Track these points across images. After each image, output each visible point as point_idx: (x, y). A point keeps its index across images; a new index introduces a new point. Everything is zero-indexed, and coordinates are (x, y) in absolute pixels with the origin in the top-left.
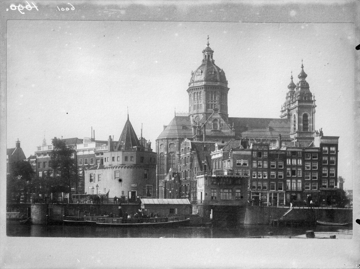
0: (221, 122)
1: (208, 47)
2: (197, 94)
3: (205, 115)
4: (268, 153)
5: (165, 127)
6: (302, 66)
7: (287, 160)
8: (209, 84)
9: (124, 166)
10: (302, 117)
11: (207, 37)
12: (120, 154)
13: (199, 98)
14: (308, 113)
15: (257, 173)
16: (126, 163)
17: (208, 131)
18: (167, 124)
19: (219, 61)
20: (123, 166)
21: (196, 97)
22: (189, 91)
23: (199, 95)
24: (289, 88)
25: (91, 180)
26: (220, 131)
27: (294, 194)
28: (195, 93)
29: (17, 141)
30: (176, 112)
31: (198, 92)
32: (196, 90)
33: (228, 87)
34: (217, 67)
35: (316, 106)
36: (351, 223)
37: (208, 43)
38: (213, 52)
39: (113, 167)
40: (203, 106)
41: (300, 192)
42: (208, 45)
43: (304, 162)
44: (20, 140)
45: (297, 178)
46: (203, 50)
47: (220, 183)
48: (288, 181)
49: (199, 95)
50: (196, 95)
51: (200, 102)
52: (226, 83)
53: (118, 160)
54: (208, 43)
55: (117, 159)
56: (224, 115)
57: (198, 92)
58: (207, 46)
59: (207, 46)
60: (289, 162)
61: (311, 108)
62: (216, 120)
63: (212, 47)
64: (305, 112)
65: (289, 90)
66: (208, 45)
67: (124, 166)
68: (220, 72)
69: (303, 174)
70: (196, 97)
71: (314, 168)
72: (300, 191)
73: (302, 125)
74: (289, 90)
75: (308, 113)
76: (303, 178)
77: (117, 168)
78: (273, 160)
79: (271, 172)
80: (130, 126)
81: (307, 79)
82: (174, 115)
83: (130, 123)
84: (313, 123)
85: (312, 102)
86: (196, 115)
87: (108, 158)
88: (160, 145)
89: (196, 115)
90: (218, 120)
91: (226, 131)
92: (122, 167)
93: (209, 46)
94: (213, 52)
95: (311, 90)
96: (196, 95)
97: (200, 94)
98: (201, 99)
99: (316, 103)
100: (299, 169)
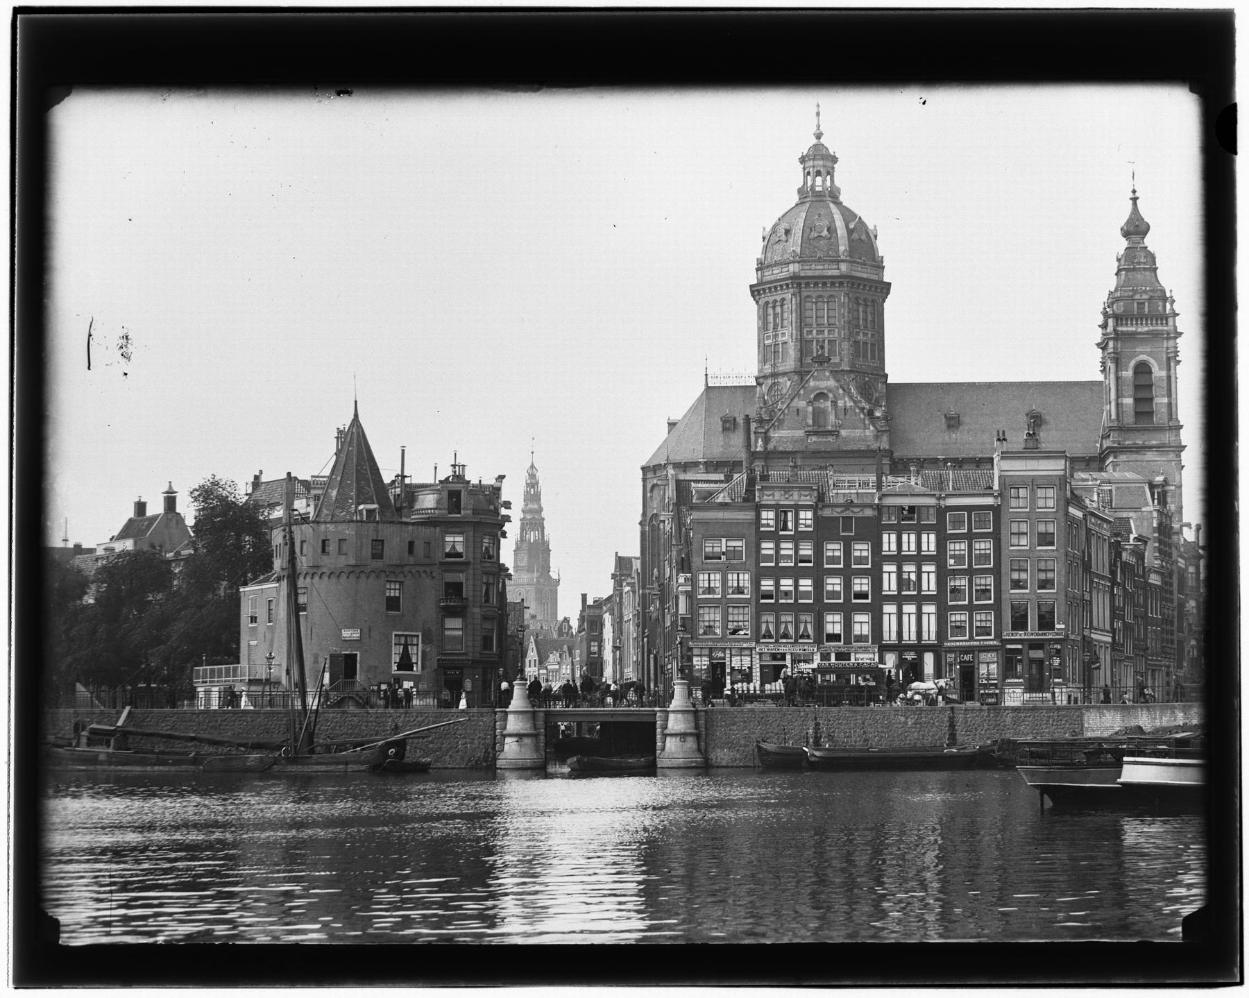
0: (840, 403)
2: (774, 307)
3: (796, 378)
4: (815, 514)
5: (672, 425)
6: (1131, 195)
7: (885, 537)
8: (810, 273)
9: (358, 570)
10: (1128, 374)
11: (815, 110)
14: (1152, 361)
17: (784, 436)
18: (677, 416)
19: (857, 190)
21: (771, 318)
23: (778, 310)
24: (1126, 234)
26: (835, 433)
27: (910, 656)
28: (767, 303)
29: (166, 489)
31: (783, 300)
33: (886, 279)
34: (848, 215)
38: (834, 159)
40: (792, 352)
41: (929, 648)
42: (819, 136)
45: (920, 600)
48: (890, 608)
49: (778, 310)
50: (770, 311)
51: (783, 334)
52: (879, 266)
53: (344, 549)
57: (783, 300)
58: (814, 141)
59: (814, 141)
60: (889, 542)
62: (821, 395)
63: (832, 144)
64: (1143, 357)
65: (1124, 243)
66: (819, 136)
67: (358, 570)
68: (852, 226)
69: (941, 583)
70: (771, 318)
73: (1128, 401)
74: (1124, 243)
75: (1152, 361)
76: (938, 599)
78: (835, 538)
79: (763, 583)
80: (358, 436)
83: (360, 427)
84: (1169, 395)
85: (1164, 318)
86: (769, 382)
88: (649, 487)
89: (769, 382)
90: (831, 395)
93: (822, 141)
94: (834, 159)
96: (770, 311)
97: (782, 306)
98: (785, 323)
100: (925, 568)
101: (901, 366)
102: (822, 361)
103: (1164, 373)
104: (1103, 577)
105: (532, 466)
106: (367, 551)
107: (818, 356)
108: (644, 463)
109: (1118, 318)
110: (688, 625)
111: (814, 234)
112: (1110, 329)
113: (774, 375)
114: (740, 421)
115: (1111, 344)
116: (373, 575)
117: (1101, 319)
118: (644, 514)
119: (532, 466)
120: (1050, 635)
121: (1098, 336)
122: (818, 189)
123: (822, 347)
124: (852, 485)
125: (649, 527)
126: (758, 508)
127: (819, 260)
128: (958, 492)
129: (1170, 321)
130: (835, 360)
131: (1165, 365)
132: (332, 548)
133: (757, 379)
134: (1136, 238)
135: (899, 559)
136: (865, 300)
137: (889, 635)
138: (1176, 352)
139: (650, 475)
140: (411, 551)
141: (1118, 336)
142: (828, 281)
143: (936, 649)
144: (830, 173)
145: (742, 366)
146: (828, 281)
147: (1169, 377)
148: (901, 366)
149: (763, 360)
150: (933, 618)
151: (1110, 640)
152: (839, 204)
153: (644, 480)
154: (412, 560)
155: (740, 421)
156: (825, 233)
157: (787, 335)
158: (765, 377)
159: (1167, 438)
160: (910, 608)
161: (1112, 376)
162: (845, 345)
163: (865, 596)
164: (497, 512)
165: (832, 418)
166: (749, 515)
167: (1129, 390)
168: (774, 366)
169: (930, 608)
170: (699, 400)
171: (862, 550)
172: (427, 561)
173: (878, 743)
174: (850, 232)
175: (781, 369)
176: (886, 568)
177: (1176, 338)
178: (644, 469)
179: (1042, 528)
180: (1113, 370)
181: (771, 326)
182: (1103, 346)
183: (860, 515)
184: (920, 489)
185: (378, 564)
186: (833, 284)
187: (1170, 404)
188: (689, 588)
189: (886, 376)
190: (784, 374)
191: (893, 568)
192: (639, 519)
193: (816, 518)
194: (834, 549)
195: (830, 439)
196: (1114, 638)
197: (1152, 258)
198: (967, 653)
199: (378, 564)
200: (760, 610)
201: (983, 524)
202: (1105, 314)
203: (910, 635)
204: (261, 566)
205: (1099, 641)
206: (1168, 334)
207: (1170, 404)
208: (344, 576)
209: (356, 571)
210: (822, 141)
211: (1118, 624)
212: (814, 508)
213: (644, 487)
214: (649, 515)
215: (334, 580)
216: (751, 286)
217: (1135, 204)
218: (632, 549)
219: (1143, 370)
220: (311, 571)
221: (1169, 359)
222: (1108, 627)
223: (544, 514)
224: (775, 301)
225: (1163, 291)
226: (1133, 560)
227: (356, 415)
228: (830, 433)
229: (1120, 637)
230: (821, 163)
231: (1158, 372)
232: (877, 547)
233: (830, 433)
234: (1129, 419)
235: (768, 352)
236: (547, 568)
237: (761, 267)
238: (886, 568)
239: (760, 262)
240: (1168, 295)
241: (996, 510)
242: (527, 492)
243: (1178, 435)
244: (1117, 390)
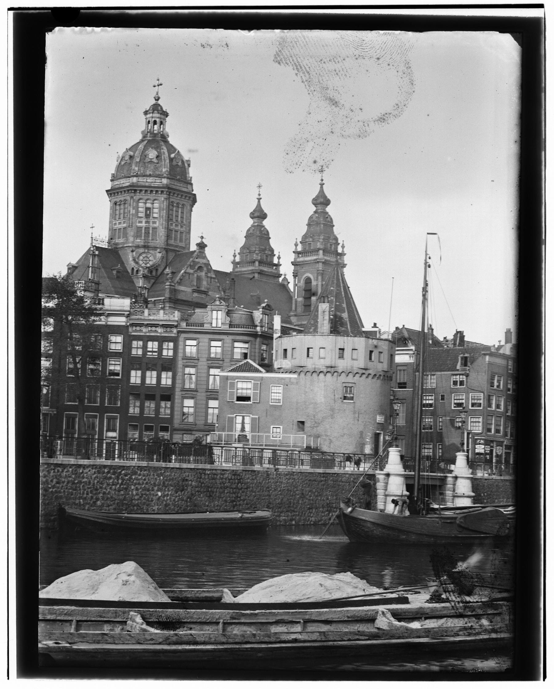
16: (370, 365)
19: (178, 136)
20: (364, 372)
24: (252, 216)
32: (181, 198)
35: (281, 265)
37: (157, 94)
38: (166, 115)
39: (340, 371)
47: (122, 471)
54: (157, 94)
55: (292, 355)
59: (154, 102)
61: (423, 288)
65: (250, 222)
66: (157, 99)
68: (173, 156)
74: (250, 222)
77: (351, 375)
82: (90, 242)
89: (141, 250)
93: (159, 102)
94: (166, 115)
99: (346, 260)
122: (155, 132)
136: (178, 204)
163: (118, 374)
173: (295, 631)
186: (157, 191)
210: (159, 102)
220: (361, 371)
230: (158, 115)
237: (114, 178)
239: (113, 175)
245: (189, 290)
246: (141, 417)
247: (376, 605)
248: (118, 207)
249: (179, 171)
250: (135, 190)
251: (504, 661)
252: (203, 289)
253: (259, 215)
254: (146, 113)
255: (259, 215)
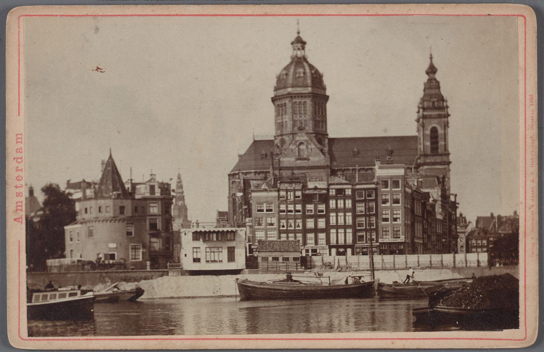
0: (310, 147)
1: (299, 37)
10: (428, 132)
12: (110, 202)
13: (284, 112)
15: (295, 222)
19: (315, 56)
21: (281, 112)
22: (274, 100)
24: (427, 73)
25: (71, 240)
30: (255, 134)
34: (311, 67)
36: (29, 273)
42: (298, 33)
43: (354, 203)
44: (33, 186)
46: (291, 42)
48: (333, 231)
52: (324, 89)
56: (320, 135)
59: (296, 35)
66: (298, 33)
70: (281, 112)
71: (320, 211)
72: (351, 245)
73: (428, 144)
78: (310, 203)
81: (438, 76)
83: (112, 159)
86: (280, 138)
87: (91, 208)
91: (317, 159)
92: (96, 221)
95: (444, 92)
96: (281, 109)
101: (334, 130)
102: (301, 129)
103: (443, 132)
104: (419, 217)
105: (179, 174)
106: (118, 211)
107: (300, 127)
108: (229, 173)
109: (424, 109)
110: (251, 240)
111: (297, 75)
112: (421, 113)
113: (282, 135)
114: (269, 154)
115: (421, 120)
116: (109, 221)
117: (417, 109)
118: (229, 193)
119: (179, 174)
120: (399, 240)
121: (415, 116)
123: (302, 123)
124: (316, 184)
125: (232, 199)
126: (279, 191)
127: (300, 86)
128: (360, 183)
129: (446, 110)
130: (307, 128)
131: (443, 127)
132: (103, 210)
133: (275, 137)
134: (432, 75)
135: (337, 210)
137: (333, 241)
138: (448, 123)
139: (231, 177)
140: (100, 211)
141: (424, 117)
142: (304, 90)
143: (351, 247)
144: (303, 48)
145: (267, 130)
146: (304, 90)
147: (445, 133)
148: (334, 130)
149: (277, 129)
150: (351, 234)
151: (422, 242)
152: (307, 62)
153: (229, 180)
154: (137, 215)
155: (269, 154)
156: (302, 75)
157: (287, 118)
158: (278, 136)
159: (445, 159)
160: (341, 231)
161: (422, 133)
162: (311, 122)
163: (323, 211)
164: (170, 194)
165: (306, 152)
166: (275, 194)
167: (429, 138)
168: (282, 131)
169: (349, 231)
170: (251, 146)
171: (322, 207)
172: (143, 214)
174: (312, 74)
175: (284, 133)
176: (331, 214)
177: (447, 117)
178: (229, 175)
179: (395, 197)
180: (422, 131)
181: (281, 114)
182: (418, 121)
183: (320, 193)
184: (344, 181)
185: (122, 216)
187: (445, 145)
188: (251, 224)
189: (328, 135)
190: (286, 134)
191: (334, 214)
192: (228, 195)
193: (303, 195)
194: (310, 207)
195: (306, 161)
196: (423, 241)
197: (438, 83)
198: (365, 248)
199: (122, 216)
200: (280, 232)
201: (370, 196)
202: (419, 108)
203: (341, 241)
204: (72, 218)
205: (418, 243)
206: (445, 115)
207: (445, 145)
208: (109, 221)
209: (114, 219)
211: (425, 236)
212: (301, 190)
213: (229, 182)
214: (231, 194)
215: (121, 222)
216: (272, 98)
217: (431, 61)
218: (225, 208)
219: (434, 131)
221: (445, 126)
222: (421, 237)
223: (184, 194)
224: (282, 104)
225: (443, 97)
226: (431, 209)
227: (111, 155)
228: (305, 159)
229: (426, 241)
231: (440, 131)
232: (327, 206)
233: (305, 159)
234: (429, 151)
235: (280, 126)
236: (186, 216)
237: (276, 89)
238: (331, 214)
240: (445, 98)
241: (376, 189)
242: (177, 185)
243: (448, 157)
244: (424, 138)
245: (293, 159)
246: (482, 240)
247: (518, 307)
248: (281, 109)
249: (317, 79)
250: (292, 97)
251: (210, 248)
252: (305, 157)
253: (432, 70)
254: (292, 43)
255: (432, 70)
